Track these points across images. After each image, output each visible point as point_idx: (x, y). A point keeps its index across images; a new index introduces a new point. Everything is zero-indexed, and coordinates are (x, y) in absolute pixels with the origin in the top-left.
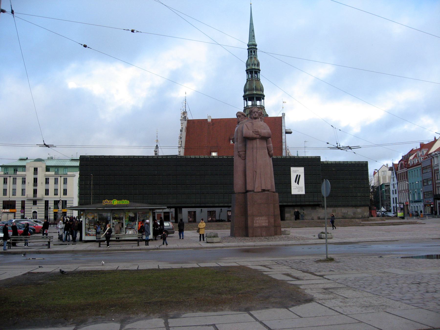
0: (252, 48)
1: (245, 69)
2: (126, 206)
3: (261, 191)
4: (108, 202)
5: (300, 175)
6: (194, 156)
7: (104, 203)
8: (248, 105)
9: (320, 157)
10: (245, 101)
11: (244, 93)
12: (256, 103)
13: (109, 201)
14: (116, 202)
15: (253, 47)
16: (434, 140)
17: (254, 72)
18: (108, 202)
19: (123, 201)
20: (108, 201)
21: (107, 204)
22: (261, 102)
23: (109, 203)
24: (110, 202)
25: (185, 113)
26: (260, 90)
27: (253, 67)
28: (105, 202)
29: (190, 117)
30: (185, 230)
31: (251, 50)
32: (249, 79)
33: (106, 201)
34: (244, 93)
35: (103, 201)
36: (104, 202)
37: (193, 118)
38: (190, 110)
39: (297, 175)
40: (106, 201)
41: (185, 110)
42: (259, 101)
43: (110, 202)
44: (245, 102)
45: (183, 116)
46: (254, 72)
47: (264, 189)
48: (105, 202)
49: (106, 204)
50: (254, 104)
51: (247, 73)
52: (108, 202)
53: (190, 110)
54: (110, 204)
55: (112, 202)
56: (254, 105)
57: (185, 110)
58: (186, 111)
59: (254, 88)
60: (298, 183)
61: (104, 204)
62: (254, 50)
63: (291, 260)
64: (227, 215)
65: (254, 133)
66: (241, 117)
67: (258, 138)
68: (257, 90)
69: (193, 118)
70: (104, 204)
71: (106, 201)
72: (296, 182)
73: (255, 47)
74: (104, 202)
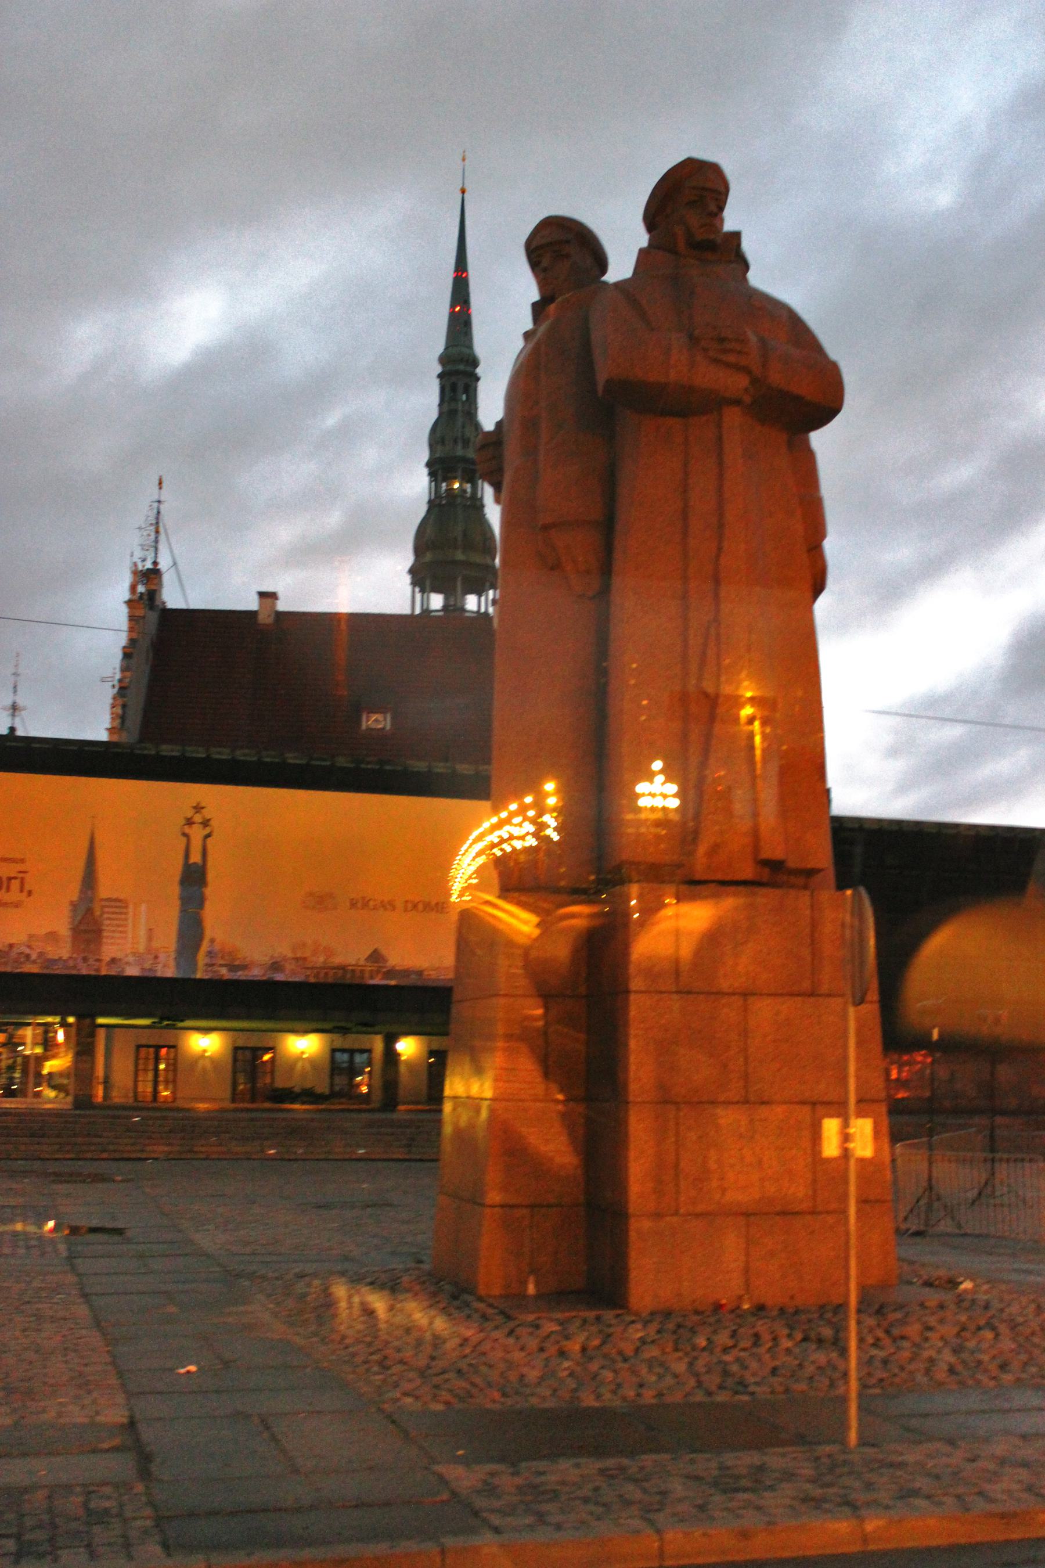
0: (457, 373)
3: (747, 871)
6: (179, 748)
8: (428, 604)
10: (417, 589)
12: (463, 600)
15: (461, 367)
16: (862, 890)
22: (483, 599)
25: (151, 576)
27: (459, 452)
29: (173, 598)
31: (453, 379)
32: (438, 501)
37: (186, 601)
38: (181, 566)
41: (155, 563)
42: (477, 594)
44: (418, 596)
45: (141, 589)
47: (778, 854)
50: (455, 605)
53: (175, 564)
56: (453, 609)
57: (155, 563)
58: (158, 567)
59: (460, 538)
64: (260, 1049)
65: (705, 350)
66: (568, 256)
67: (737, 402)
69: (186, 601)
73: (469, 369)
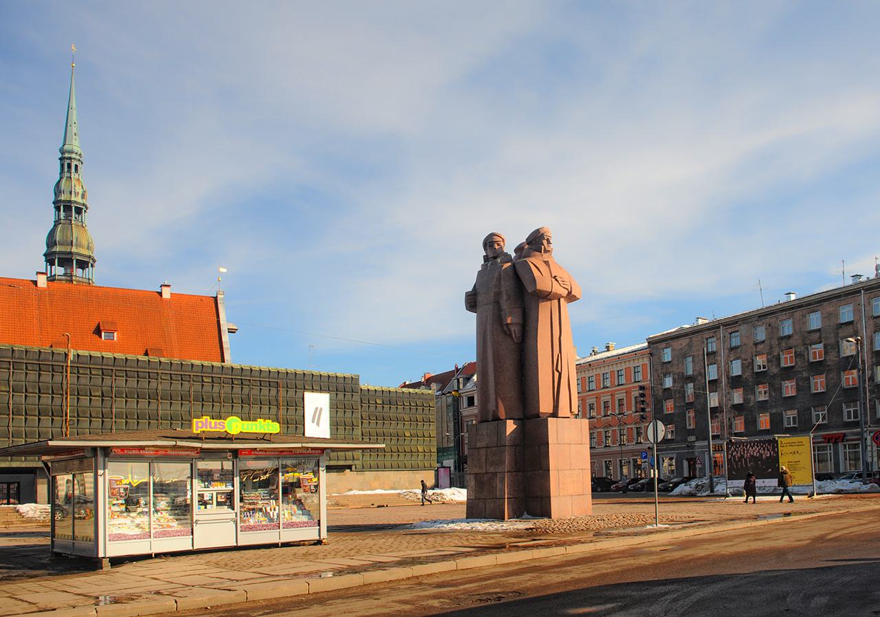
1: (53, 199)
2: (263, 438)
4: (213, 426)
5: (321, 409)
7: (197, 427)
9: (359, 376)
11: (46, 248)
13: (215, 423)
14: (237, 426)
17: (75, 261)
18: (213, 426)
19: (260, 423)
20: (213, 421)
21: (209, 429)
23: (215, 427)
24: (218, 426)
26: (86, 246)
28: (200, 425)
30: (461, 503)
33: (206, 419)
34: (48, 247)
35: (195, 420)
36: (197, 422)
39: (317, 408)
40: (206, 419)
43: (218, 426)
44: (49, 267)
46: (75, 261)
48: (200, 425)
49: (204, 429)
51: (58, 209)
52: (210, 422)
54: (218, 430)
55: (226, 425)
60: (318, 424)
61: (197, 430)
62: (77, 163)
63: (420, 548)
68: (80, 246)
70: (197, 430)
71: (204, 420)
72: (313, 422)
74: (197, 422)
